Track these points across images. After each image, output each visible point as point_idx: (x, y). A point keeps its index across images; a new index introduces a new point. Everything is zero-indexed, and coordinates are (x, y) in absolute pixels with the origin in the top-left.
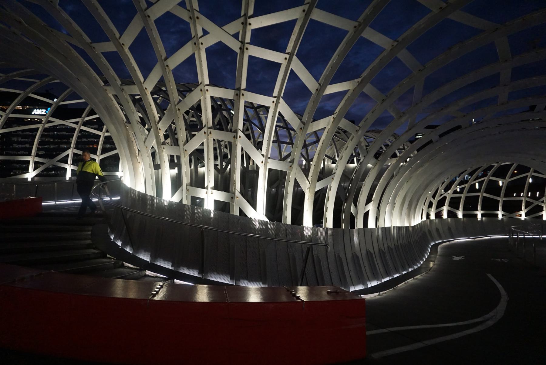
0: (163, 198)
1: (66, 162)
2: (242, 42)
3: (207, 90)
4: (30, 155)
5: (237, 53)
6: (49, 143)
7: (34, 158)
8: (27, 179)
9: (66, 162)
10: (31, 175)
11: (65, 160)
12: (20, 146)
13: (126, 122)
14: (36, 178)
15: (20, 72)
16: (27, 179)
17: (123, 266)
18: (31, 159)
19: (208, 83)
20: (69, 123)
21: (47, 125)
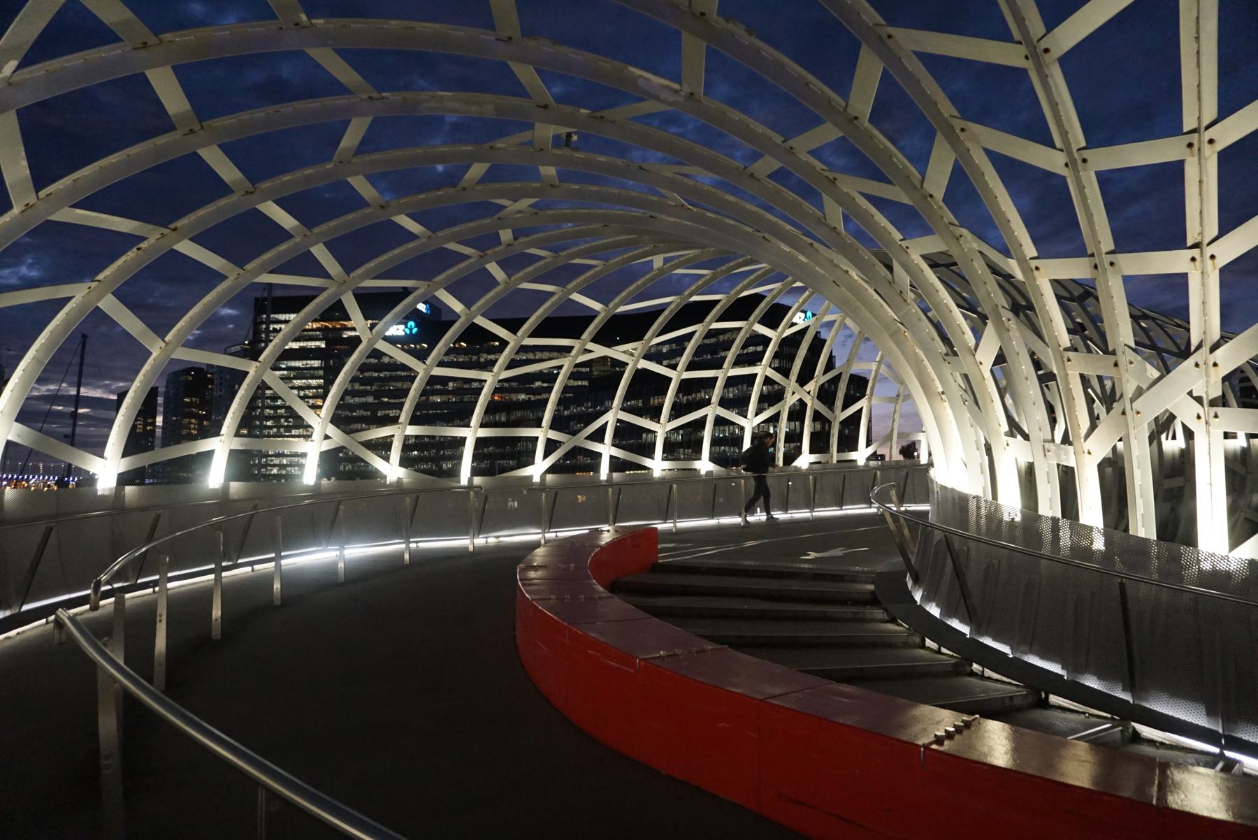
0: (1200, 547)
1: (601, 440)
2: (1067, 149)
3: (1037, 268)
4: (539, 426)
5: (1064, 178)
6: (391, 394)
7: (476, 431)
8: (531, 477)
9: (601, 440)
10: (537, 469)
11: (598, 436)
12: (357, 399)
13: (947, 354)
14: (549, 477)
15: (535, 236)
16: (531, 477)
17: (1045, 704)
18: (542, 434)
19: (1035, 254)
20: (617, 353)
21: (582, 359)
